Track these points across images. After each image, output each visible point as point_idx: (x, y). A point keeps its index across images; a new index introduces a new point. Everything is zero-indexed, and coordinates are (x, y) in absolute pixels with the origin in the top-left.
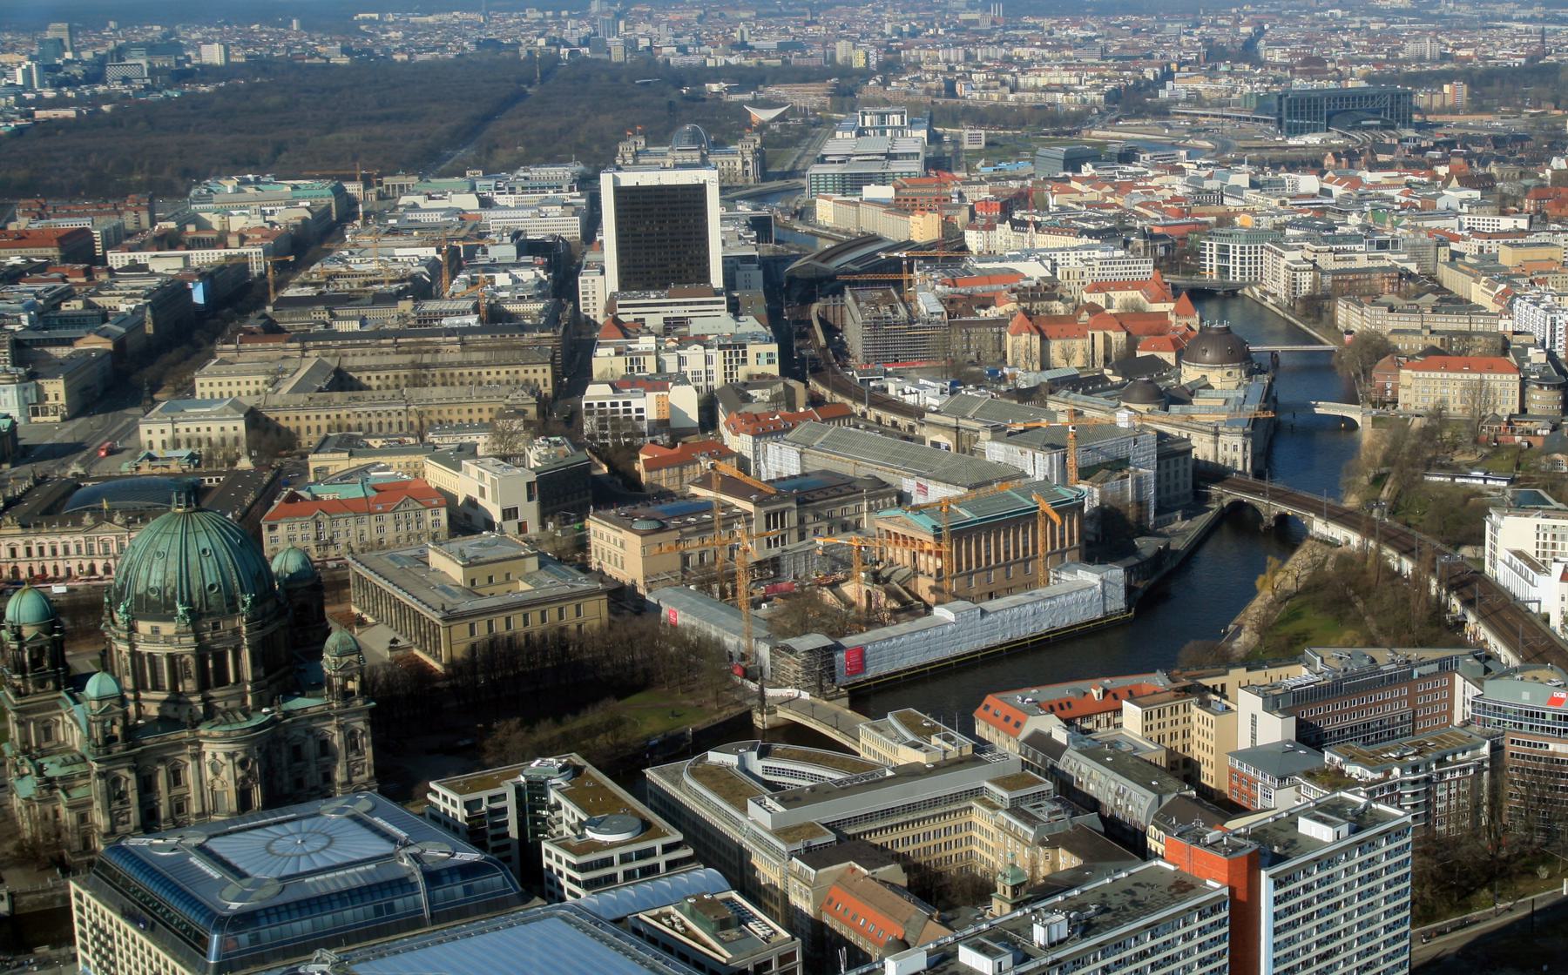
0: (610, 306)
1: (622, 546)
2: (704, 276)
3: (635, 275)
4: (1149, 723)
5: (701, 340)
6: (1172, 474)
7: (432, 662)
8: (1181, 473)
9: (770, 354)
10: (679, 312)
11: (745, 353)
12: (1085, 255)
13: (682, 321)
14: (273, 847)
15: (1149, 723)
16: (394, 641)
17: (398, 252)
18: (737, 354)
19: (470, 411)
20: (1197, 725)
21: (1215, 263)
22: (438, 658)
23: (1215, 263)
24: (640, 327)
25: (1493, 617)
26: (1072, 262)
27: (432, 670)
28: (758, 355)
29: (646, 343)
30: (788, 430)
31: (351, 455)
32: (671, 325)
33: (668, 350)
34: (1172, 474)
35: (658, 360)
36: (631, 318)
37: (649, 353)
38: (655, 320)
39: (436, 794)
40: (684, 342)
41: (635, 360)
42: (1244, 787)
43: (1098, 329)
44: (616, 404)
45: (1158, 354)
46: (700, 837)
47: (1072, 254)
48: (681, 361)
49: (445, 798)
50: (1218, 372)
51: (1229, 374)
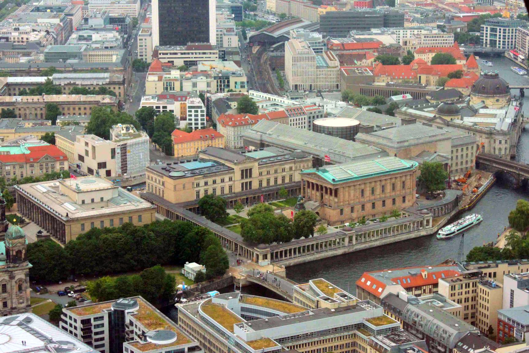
0: (156, 54)
1: (163, 184)
2: (207, 39)
3: (168, 38)
4: (453, 292)
5: (205, 73)
6: (465, 155)
7: (59, 243)
8: (470, 155)
9: (242, 83)
10: (192, 57)
11: (228, 82)
12: (416, 32)
13: (194, 63)
14: (7, 338)
15: (453, 292)
16: (40, 232)
17: (39, 20)
18: (224, 82)
19: (80, 109)
20: (480, 294)
21: (488, 38)
22: (64, 242)
23: (488, 38)
24: (171, 65)
25: (120, 323)
26: (408, 35)
27: (61, 247)
28: (236, 83)
29: (175, 74)
30: (253, 124)
31: (16, 132)
32: (189, 65)
33: (187, 79)
34: (465, 155)
35: (181, 84)
36: (166, 61)
37: (177, 80)
38: (179, 62)
39: (66, 315)
40: (196, 74)
41: (169, 86)
42: (507, 330)
43: (423, 73)
44: (159, 107)
45: (456, 89)
46: (207, 344)
47: (409, 31)
48: (195, 85)
49: (71, 318)
50: (492, 100)
51: (497, 101)
